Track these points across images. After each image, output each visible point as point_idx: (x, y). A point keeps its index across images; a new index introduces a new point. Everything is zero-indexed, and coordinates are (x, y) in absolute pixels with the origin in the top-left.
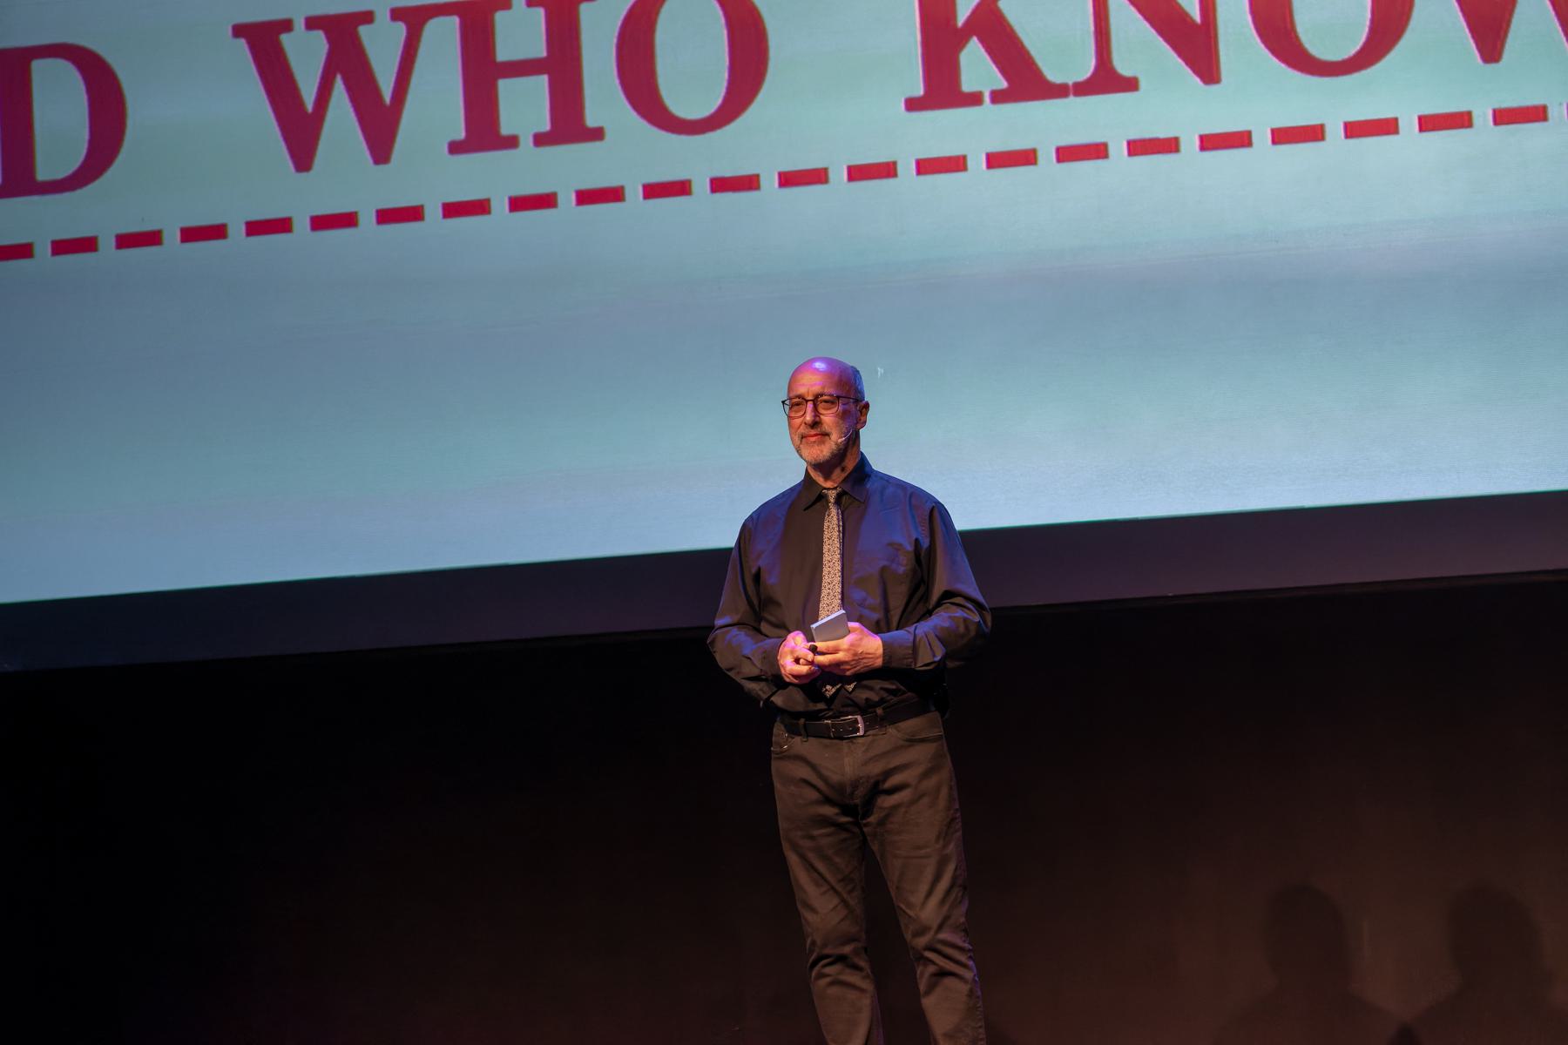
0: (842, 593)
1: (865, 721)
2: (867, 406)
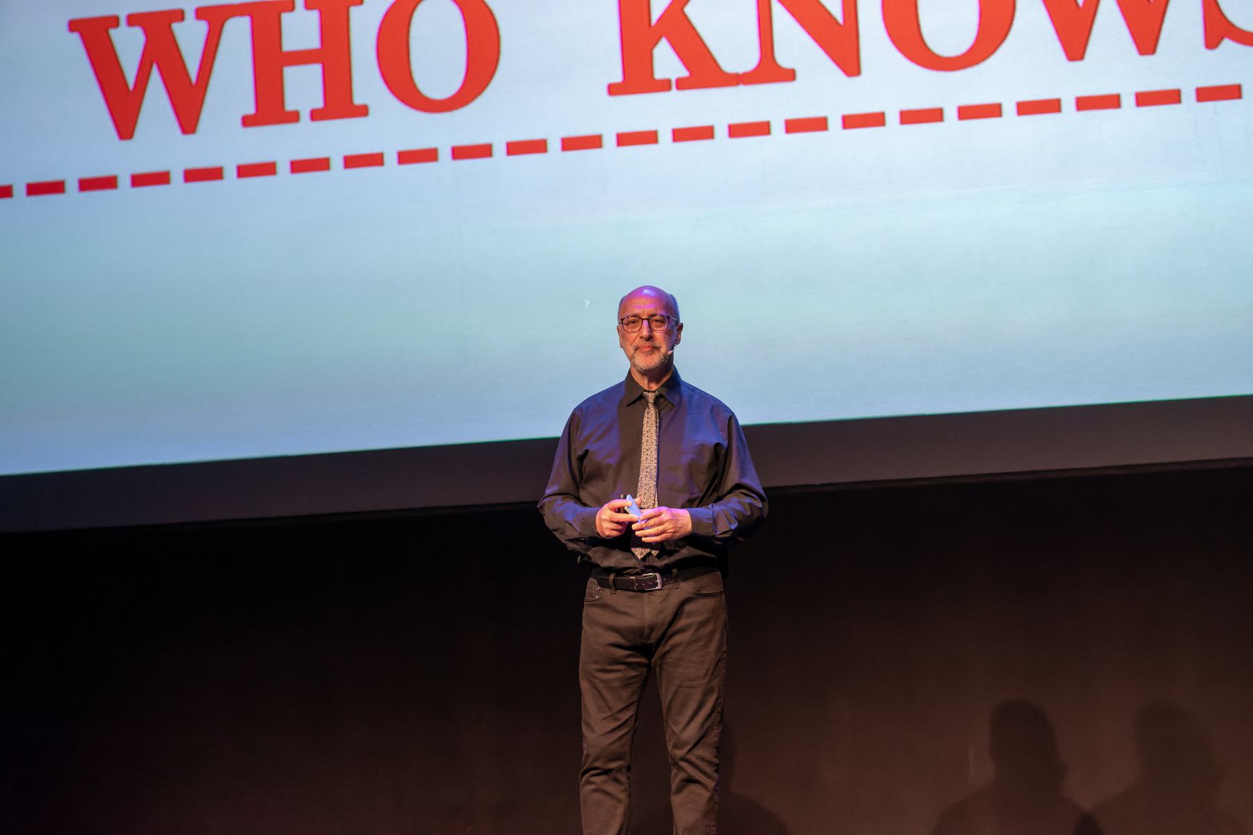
2: (681, 327)
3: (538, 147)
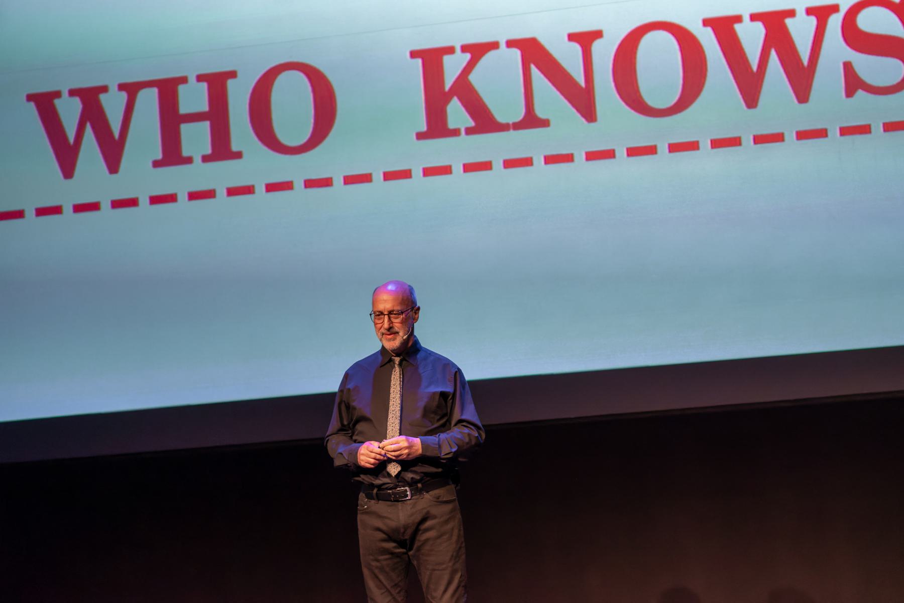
0: (401, 416)
1: (411, 491)
2: (419, 309)
3: (366, 178)
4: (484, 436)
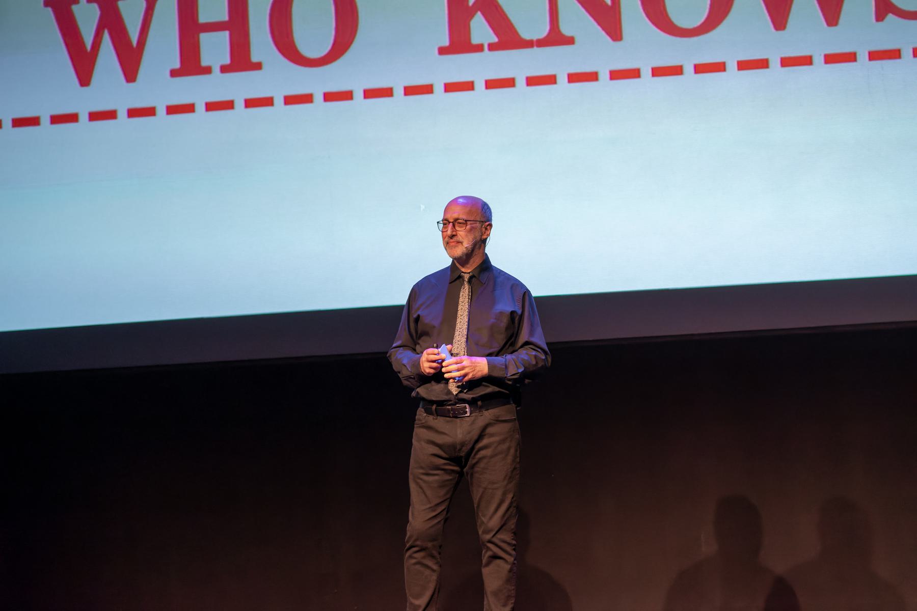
4: (550, 359)
